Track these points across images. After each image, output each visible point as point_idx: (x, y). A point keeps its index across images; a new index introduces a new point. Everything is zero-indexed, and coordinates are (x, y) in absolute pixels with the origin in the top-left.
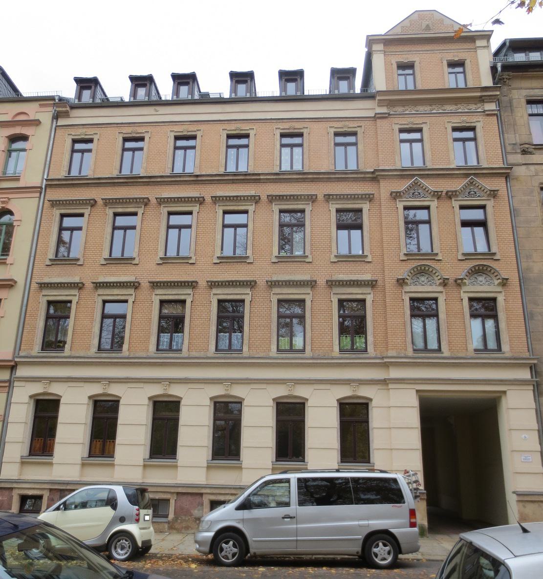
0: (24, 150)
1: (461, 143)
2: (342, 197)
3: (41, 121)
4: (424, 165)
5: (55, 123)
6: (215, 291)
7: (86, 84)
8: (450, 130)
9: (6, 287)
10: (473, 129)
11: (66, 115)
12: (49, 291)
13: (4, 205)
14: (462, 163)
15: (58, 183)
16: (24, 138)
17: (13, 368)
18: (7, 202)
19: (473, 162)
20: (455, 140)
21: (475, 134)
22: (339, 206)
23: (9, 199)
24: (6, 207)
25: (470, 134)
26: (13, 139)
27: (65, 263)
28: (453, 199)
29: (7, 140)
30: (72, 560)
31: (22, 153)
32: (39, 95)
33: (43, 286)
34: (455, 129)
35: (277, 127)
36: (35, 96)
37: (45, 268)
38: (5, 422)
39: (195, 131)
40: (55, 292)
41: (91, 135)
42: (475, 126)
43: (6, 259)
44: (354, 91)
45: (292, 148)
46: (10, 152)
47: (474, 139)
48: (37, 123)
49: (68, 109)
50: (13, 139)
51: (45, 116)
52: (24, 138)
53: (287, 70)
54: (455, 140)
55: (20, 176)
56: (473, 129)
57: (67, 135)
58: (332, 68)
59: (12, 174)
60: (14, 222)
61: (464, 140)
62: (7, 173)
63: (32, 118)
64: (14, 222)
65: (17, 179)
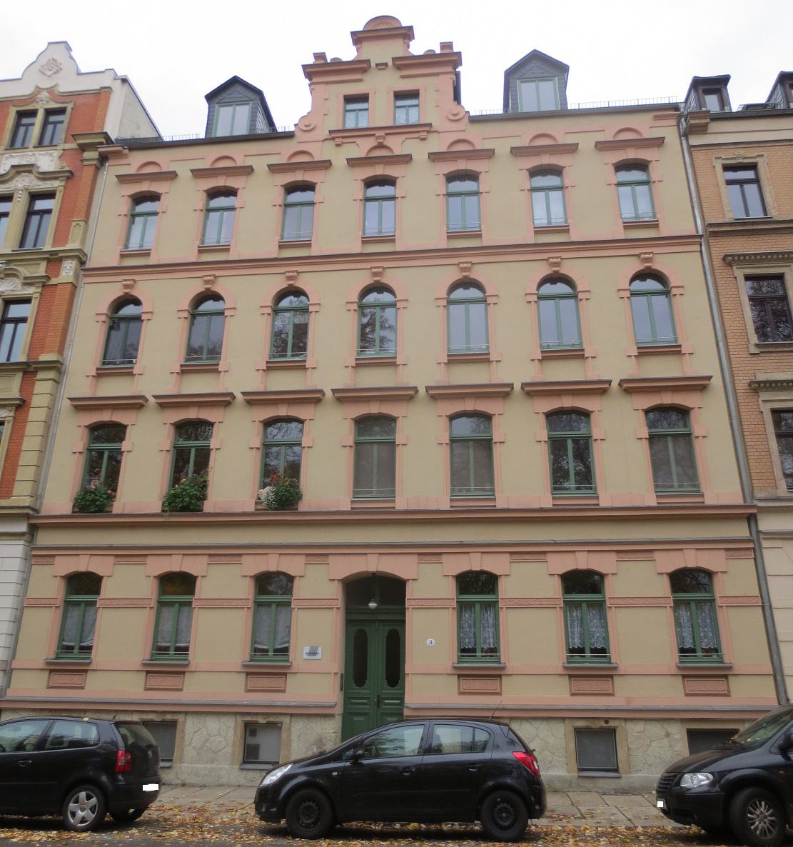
0: (155, 214)
1: (737, 187)
2: (742, 258)
3: (178, 173)
4: (766, 214)
5: (684, 142)
6: (764, 396)
7: (714, 86)
8: (719, 169)
9: (311, 403)
10: (753, 167)
11: (703, 129)
12: (773, 393)
13: (127, 291)
14: (741, 215)
15: (729, 229)
16: (154, 197)
17: (751, 519)
18: (213, 282)
19: (756, 213)
20: (729, 182)
21: (757, 174)
22: (748, 271)
23: (216, 277)
24: (212, 289)
25: (749, 174)
26: (139, 199)
27: (782, 350)
28: (734, 267)
29: (205, 195)
30: (65, 830)
31: (150, 218)
32: (671, 102)
33: (758, 387)
34: (727, 168)
35: (716, 156)
36: (633, 104)
37: (749, 359)
38: (767, 608)
39: (755, 158)
40: (782, 396)
41: (751, 158)
42: (757, 163)
43: (132, 368)
44: (731, 109)
45: (742, 186)
46: (134, 216)
47: (757, 181)
48: (659, 142)
49: (709, 120)
50: (139, 199)
51: (670, 133)
52: (154, 197)
53: (786, 71)
54: (729, 182)
55: (229, 245)
56: (753, 167)
57: (714, 159)
58: (695, 77)
59: (650, 217)
60: (143, 315)
61: (741, 183)
62: (206, 241)
63: (239, 164)
64: (143, 315)
65: (307, 245)
